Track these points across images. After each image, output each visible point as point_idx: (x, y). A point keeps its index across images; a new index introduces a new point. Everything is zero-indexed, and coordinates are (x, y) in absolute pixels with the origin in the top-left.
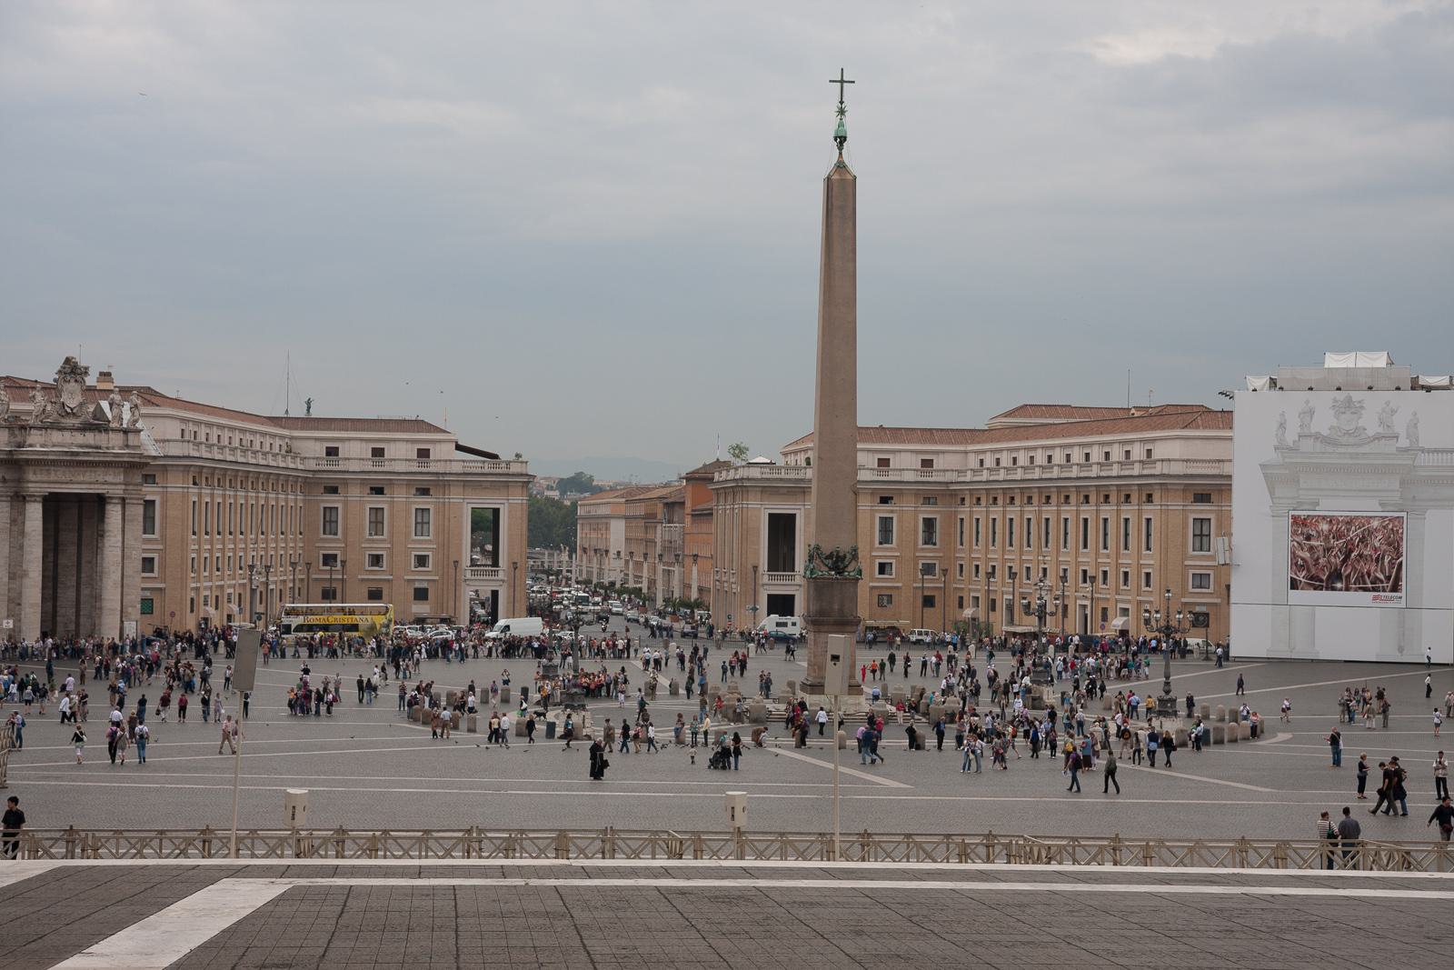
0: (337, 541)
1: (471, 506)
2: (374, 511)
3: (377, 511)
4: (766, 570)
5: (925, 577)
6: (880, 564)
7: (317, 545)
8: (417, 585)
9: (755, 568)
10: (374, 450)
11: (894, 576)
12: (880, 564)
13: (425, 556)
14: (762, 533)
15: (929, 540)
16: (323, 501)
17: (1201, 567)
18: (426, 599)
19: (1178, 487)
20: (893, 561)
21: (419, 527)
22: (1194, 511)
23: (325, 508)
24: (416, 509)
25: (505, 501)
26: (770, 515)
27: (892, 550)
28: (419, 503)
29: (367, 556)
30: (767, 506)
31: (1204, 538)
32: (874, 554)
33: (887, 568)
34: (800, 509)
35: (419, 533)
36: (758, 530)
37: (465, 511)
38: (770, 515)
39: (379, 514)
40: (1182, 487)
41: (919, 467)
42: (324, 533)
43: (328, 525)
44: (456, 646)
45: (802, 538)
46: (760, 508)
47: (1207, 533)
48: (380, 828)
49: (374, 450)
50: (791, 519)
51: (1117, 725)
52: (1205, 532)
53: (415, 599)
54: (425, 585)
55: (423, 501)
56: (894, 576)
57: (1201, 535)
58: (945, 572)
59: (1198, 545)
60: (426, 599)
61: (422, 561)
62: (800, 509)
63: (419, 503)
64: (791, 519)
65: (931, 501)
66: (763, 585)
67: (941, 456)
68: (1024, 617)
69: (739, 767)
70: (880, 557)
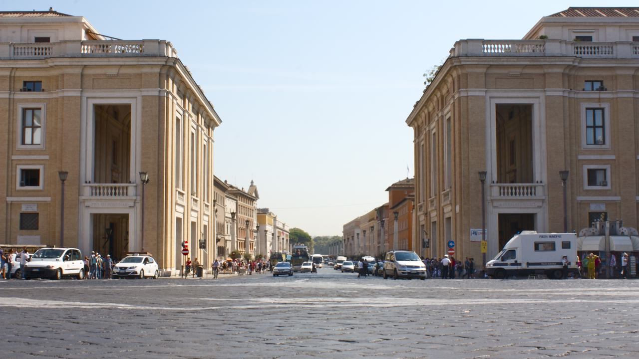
0: (604, 152)
1: (91, 102)
2: (591, 112)
4: (495, 178)
6: (589, 170)
8: (24, 209)
9: (483, 174)
11: (608, 187)
12: (589, 170)
18: (36, 227)
25: (541, 95)
30: (496, 94)
31: (592, 124)
33: (600, 177)
34: (538, 97)
36: (483, 127)
37: (488, 104)
39: (599, 113)
40: (560, 70)
45: (544, 136)
46: (484, 97)
47: (601, 124)
50: (525, 111)
52: (599, 122)
53: (22, 228)
54: (33, 209)
56: (608, 187)
57: (595, 127)
60: (36, 227)
61: (31, 177)
62: (538, 97)
63: (27, 100)
64: (525, 111)
66: (492, 201)
69: (128, 193)
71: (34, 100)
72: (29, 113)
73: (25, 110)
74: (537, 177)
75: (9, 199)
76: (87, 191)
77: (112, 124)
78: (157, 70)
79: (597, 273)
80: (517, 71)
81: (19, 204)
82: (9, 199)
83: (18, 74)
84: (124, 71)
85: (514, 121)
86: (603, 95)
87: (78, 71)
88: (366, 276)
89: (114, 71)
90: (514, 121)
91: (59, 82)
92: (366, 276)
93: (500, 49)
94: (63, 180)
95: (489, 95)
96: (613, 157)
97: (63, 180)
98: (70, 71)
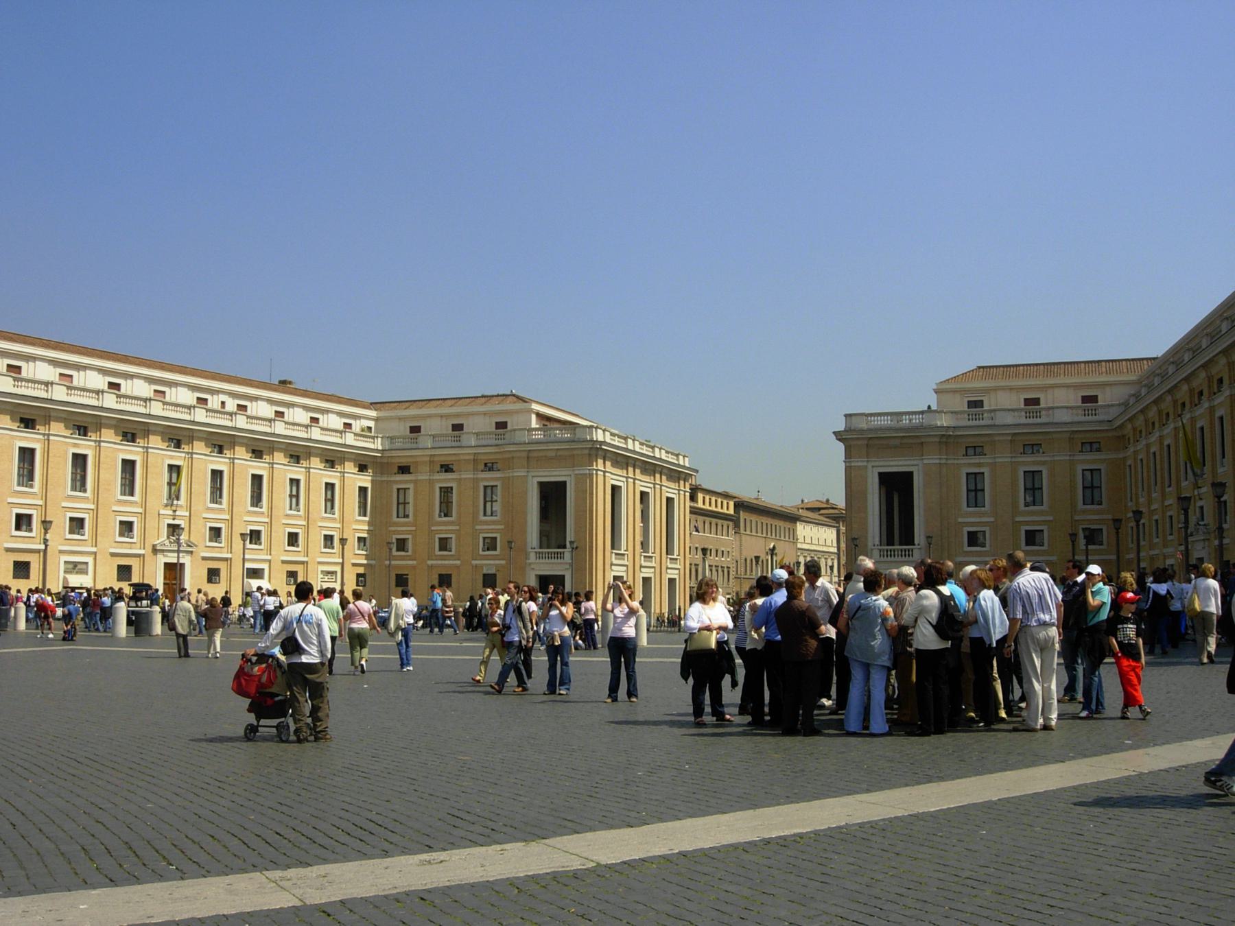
0: (983, 515)
3: (446, 492)
4: (877, 542)
5: (1090, 547)
7: (960, 520)
12: (969, 533)
13: (446, 539)
14: (870, 497)
15: (446, 510)
16: (396, 482)
17: (1034, 523)
19: (860, 442)
20: (987, 529)
21: (401, 507)
22: (1024, 463)
23: (485, 487)
24: (968, 474)
26: (880, 474)
27: (1041, 513)
28: (400, 482)
29: (1105, 542)
32: (1017, 519)
35: (401, 514)
37: (870, 474)
38: (880, 474)
40: (937, 440)
41: (1080, 404)
42: (485, 515)
43: (489, 505)
44: (59, 612)
51: (178, 635)
54: (493, 571)
55: (488, 478)
59: (1029, 499)
63: (400, 482)
65: (1095, 446)
67: (1108, 389)
68: (624, 574)
70: (1027, 523)
81: (482, 566)
85: (897, 488)
86: (983, 460)
89: (553, 454)
90: (897, 488)
91: (509, 462)
93: (886, 422)
94: (1117, 529)
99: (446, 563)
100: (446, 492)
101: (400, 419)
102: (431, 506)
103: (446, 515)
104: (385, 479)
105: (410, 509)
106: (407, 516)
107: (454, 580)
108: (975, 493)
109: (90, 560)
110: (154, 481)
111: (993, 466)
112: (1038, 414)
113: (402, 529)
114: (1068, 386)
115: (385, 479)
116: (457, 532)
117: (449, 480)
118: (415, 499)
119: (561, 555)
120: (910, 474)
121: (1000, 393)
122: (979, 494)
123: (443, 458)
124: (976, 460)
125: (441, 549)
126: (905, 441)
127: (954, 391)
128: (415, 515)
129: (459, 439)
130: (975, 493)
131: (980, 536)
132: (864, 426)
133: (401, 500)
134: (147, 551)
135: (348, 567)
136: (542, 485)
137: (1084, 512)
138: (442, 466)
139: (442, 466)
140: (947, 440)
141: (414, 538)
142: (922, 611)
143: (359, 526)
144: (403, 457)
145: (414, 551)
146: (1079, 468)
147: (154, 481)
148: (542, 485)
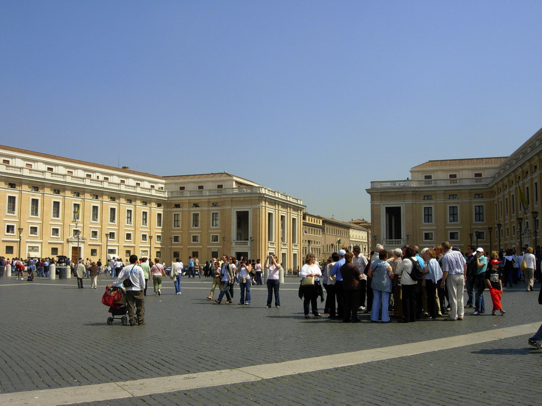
0: (432, 226)
3: (196, 216)
4: (385, 238)
5: (478, 240)
6: (425, 234)
7: (421, 228)
10: (181, 188)
12: (425, 234)
13: (196, 236)
14: (382, 218)
15: (196, 224)
16: (174, 211)
17: (454, 229)
19: (377, 194)
20: (433, 232)
21: (176, 222)
22: (449, 203)
23: (213, 214)
24: (425, 208)
26: (386, 208)
27: (457, 225)
28: (176, 211)
32: (446, 228)
35: (176, 225)
37: (382, 208)
38: (386, 208)
40: (411, 193)
41: (474, 177)
42: (213, 226)
43: (214, 221)
48: (261, 376)
49: (181, 188)
54: (216, 250)
55: (214, 209)
58: (20, 230)
59: (452, 219)
61: (215, 239)
63: (176, 211)
65: (480, 196)
67: (486, 171)
68: (274, 252)
70: (451, 229)
71: (216, 210)
72: (215, 215)
73: (213, 214)
74: (402, 238)
75: (208, 247)
76: (234, 244)
77: (243, 218)
78: (257, 198)
79: (112, 289)
80: (394, 194)
81: (211, 248)
82: (208, 247)
83: (191, 201)
84: (246, 199)
85: (394, 214)
86: (431, 202)
87: (230, 199)
88: (400, 278)
89: (242, 199)
90: (394, 214)
91: (223, 203)
92: (400, 278)
93: (389, 185)
94: (490, 232)
95: (233, 208)
96: (435, 228)
97: (490, 232)
98: (227, 199)
99: (196, 247)
100: (196, 216)
101: (176, 184)
102: (189, 222)
103: (196, 226)
104: (169, 210)
105: (180, 223)
106: (179, 226)
107: (199, 254)
108: (428, 216)
109: (39, 245)
110: (67, 211)
111: (436, 204)
112: (455, 182)
113: (176, 232)
114: (469, 169)
115: (169, 210)
116: (201, 233)
117: (197, 211)
118: (182, 219)
119: (246, 244)
120: (400, 208)
121: (439, 172)
122: (430, 216)
123: (194, 201)
124: (428, 202)
125: (194, 241)
126: (397, 193)
127: (419, 172)
128: (182, 226)
129: (201, 192)
130: (428, 216)
131: (430, 235)
132: (379, 187)
133: (176, 219)
134: (64, 242)
135: (153, 249)
136: (238, 213)
137: (476, 224)
138: (194, 204)
139: (194, 204)
140: (415, 193)
141: (182, 236)
142: (405, 268)
143: (158, 231)
144: (177, 200)
145: (182, 242)
146: (474, 205)
147: (67, 211)
148: (238, 213)
